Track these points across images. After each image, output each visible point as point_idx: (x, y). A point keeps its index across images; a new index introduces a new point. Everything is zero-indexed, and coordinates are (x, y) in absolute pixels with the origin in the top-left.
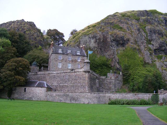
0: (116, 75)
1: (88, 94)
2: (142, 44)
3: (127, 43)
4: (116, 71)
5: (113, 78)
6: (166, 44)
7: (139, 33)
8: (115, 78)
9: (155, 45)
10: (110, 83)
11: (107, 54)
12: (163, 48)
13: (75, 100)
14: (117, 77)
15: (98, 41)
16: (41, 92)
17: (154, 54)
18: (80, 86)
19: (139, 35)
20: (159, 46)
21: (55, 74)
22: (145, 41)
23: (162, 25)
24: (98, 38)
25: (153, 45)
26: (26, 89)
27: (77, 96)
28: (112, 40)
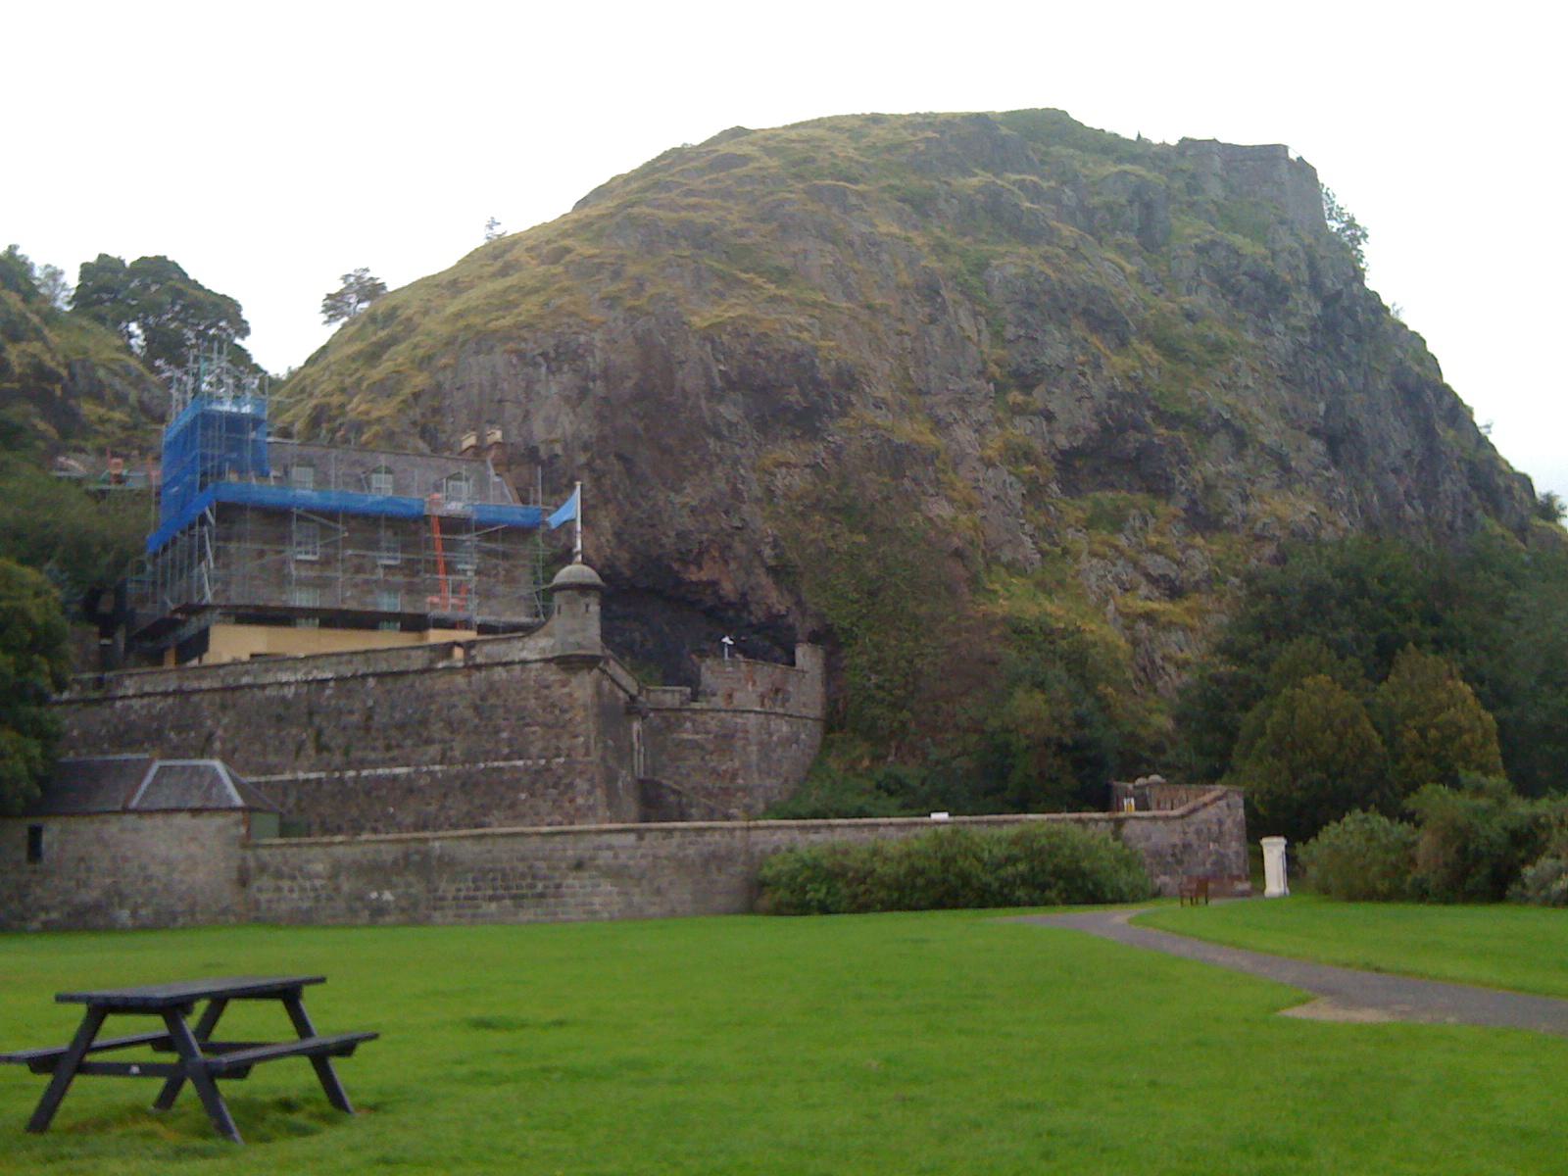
0: (767, 674)
1: (614, 840)
2: (957, 413)
3: (845, 407)
4: (769, 642)
5: (747, 697)
6: (1150, 407)
7: (933, 321)
8: (762, 697)
9: (1061, 417)
10: (726, 739)
11: (678, 499)
12: (1133, 440)
13: (514, 897)
14: (777, 691)
15: (598, 388)
16: (194, 848)
17: (1054, 487)
18: (526, 780)
19: (936, 333)
20: (1095, 426)
21: (289, 692)
22: (980, 383)
23: (1120, 247)
24: (594, 364)
25: (1049, 417)
26: (46, 838)
27: (523, 859)
28: (719, 383)
